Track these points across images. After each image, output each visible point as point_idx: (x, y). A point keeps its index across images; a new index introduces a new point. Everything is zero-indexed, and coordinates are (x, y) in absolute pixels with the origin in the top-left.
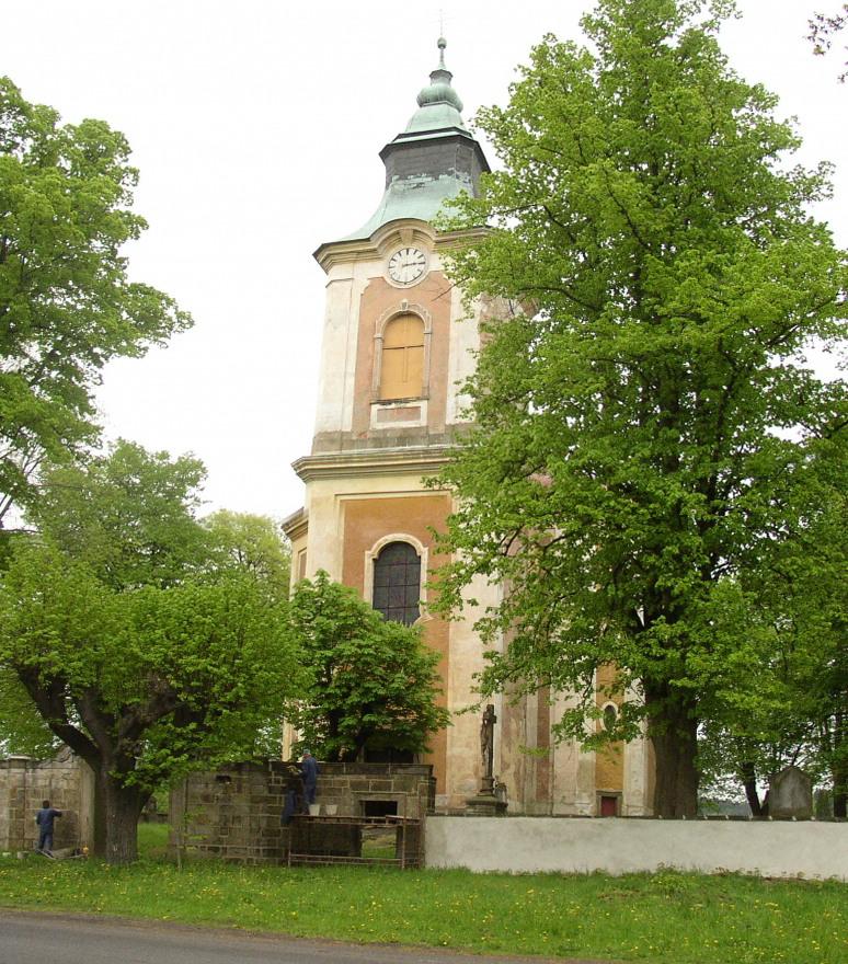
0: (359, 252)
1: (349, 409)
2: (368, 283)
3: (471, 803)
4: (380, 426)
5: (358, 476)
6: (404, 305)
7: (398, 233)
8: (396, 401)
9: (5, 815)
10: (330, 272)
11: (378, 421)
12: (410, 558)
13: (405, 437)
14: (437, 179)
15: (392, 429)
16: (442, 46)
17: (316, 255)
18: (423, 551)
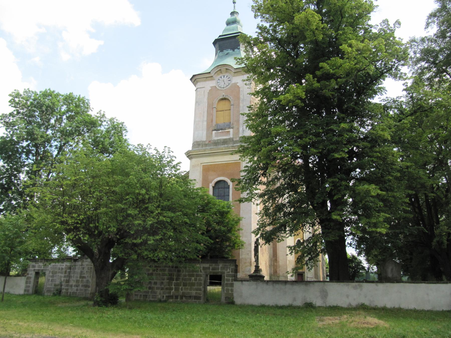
0: (207, 78)
1: (205, 132)
2: (210, 88)
3: (251, 276)
4: (216, 138)
5: (210, 156)
6: (223, 96)
7: (220, 70)
8: (221, 129)
9: (138, 336)
10: (197, 85)
11: (215, 136)
12: (226, 186)
13: (225, 142)
14: (234, 51)
15: (220, 140)
16: (234, 3)
17: (191, 79)
18: (230, 184)
